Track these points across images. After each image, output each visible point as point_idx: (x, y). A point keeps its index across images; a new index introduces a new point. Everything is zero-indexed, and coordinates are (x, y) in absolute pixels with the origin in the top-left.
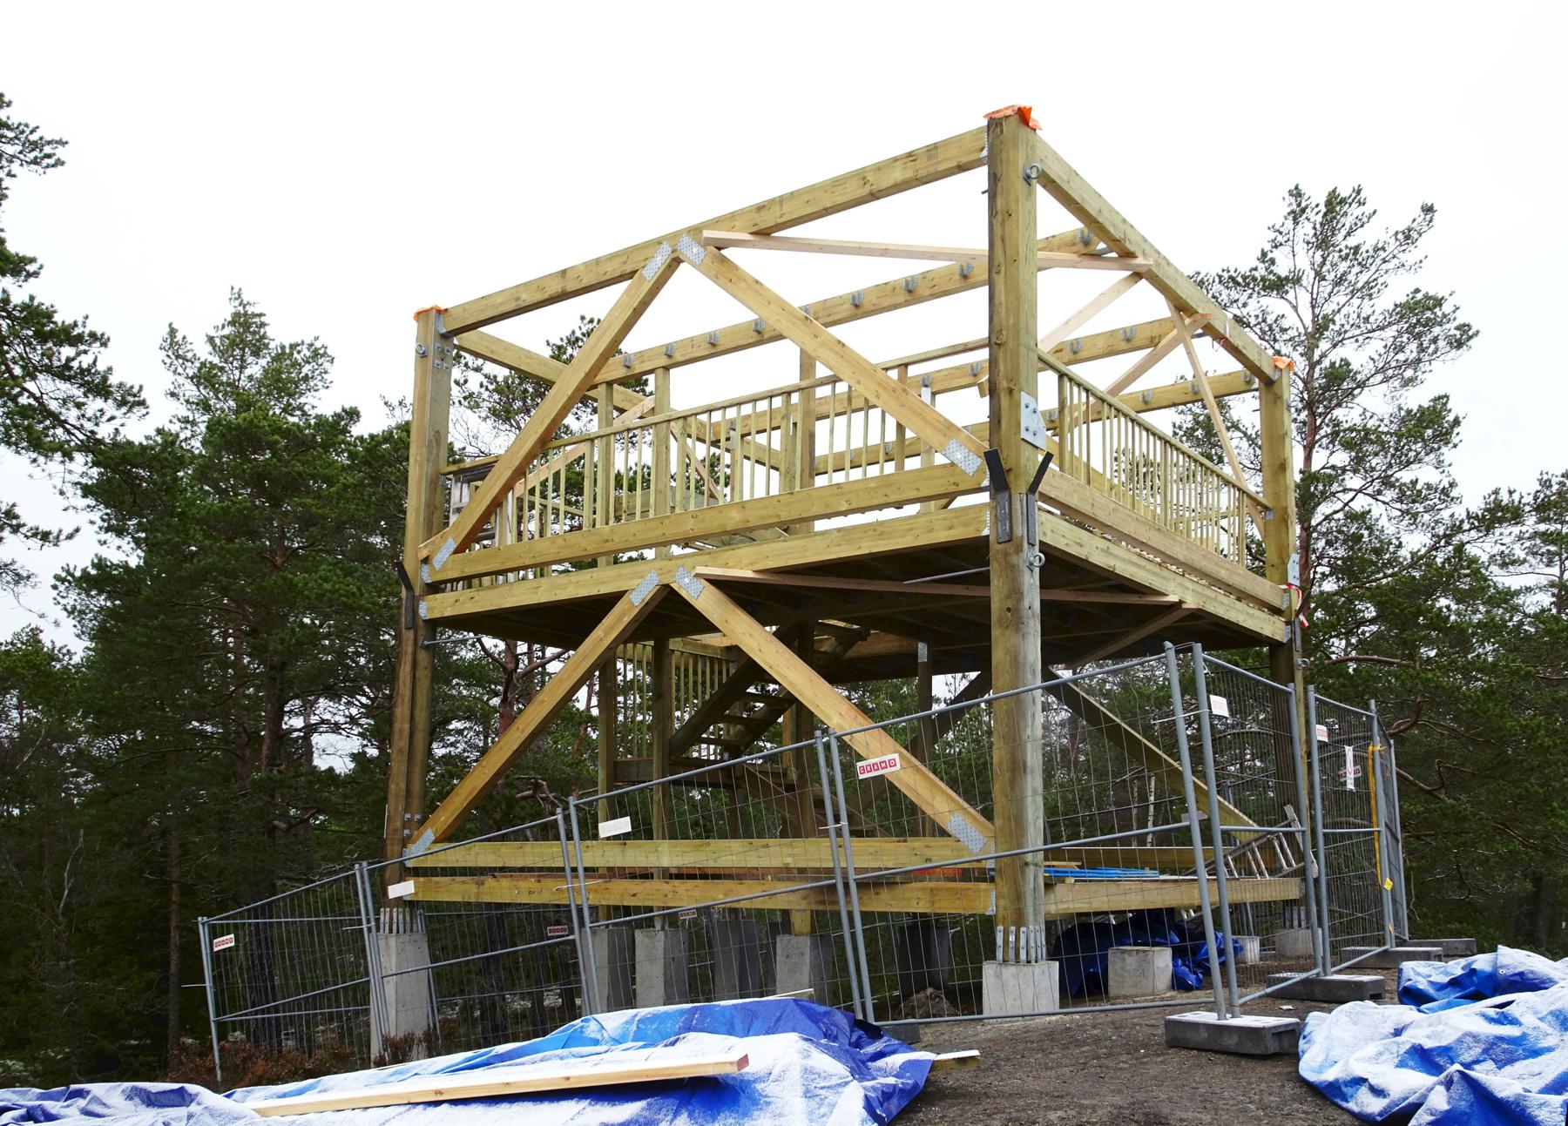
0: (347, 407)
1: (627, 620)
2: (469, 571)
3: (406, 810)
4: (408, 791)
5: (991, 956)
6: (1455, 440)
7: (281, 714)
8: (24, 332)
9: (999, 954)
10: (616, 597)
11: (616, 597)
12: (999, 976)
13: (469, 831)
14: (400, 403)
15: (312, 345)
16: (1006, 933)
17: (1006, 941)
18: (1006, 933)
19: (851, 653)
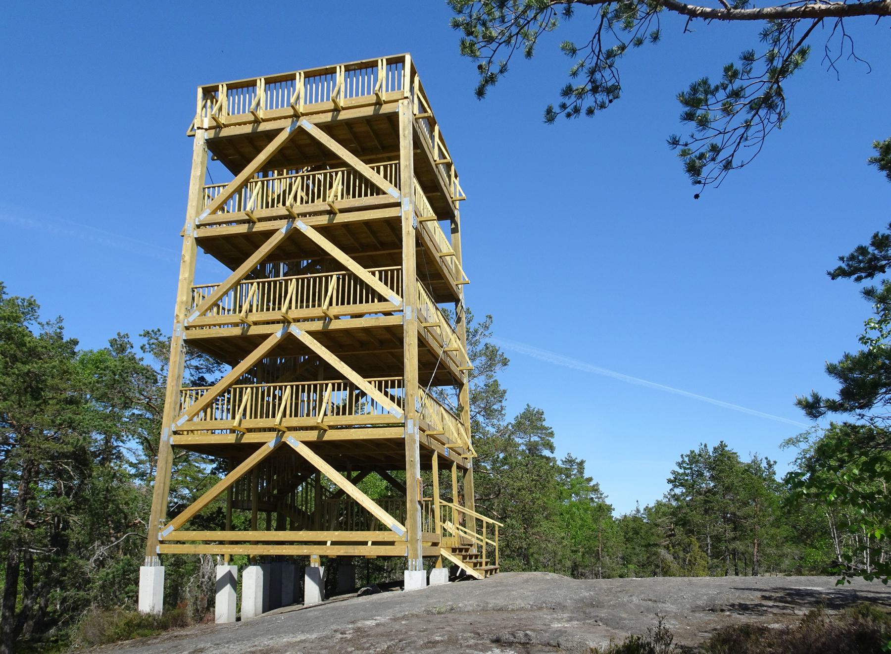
0: (72, 339)
1: (267, 452)
2: (193, 428)
3: (160, 518)
4: (161, 510)
5: (407, 569)
6: (497, 348)
7: (304, 513)
8: (691, 498)
9: (410, 568)
10: (263, 444)
11: (263, 444)
12: (410, 576)
13: (211, 527)
14: (47, 323)
15: (29, 300)
16: (412, 561)
17: (412, 564)
18: (412, 561)
19: (886, 577)
